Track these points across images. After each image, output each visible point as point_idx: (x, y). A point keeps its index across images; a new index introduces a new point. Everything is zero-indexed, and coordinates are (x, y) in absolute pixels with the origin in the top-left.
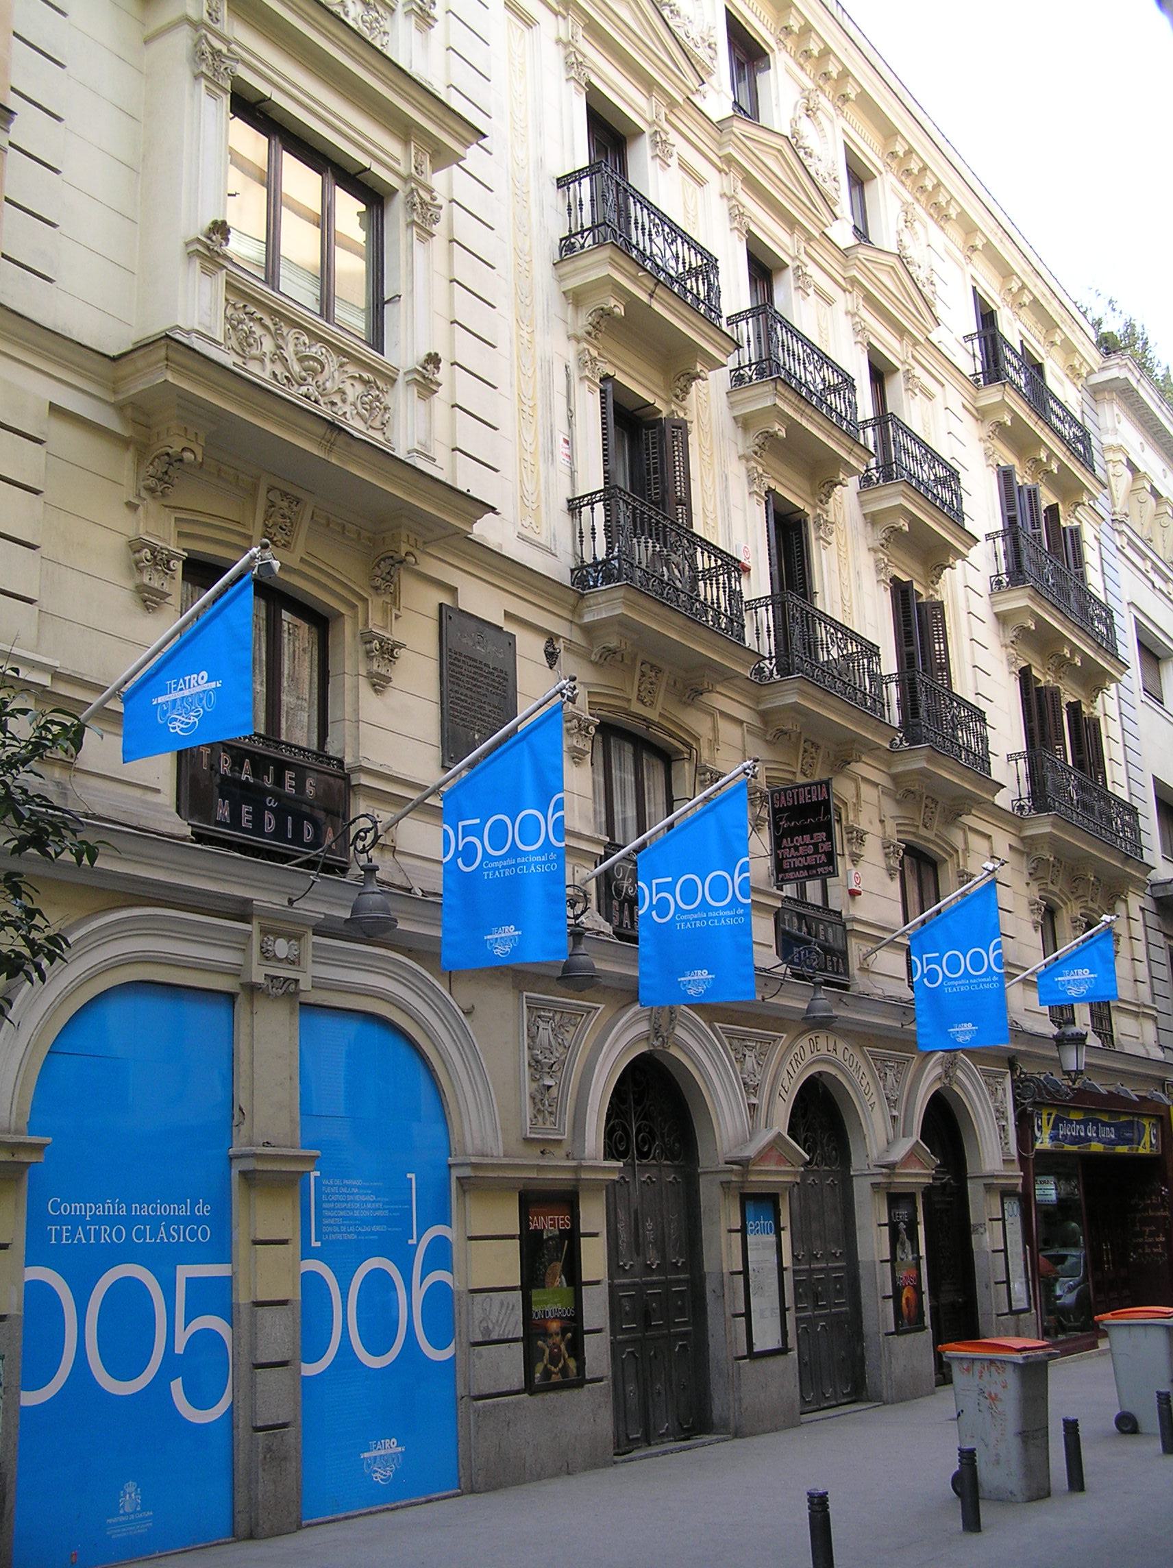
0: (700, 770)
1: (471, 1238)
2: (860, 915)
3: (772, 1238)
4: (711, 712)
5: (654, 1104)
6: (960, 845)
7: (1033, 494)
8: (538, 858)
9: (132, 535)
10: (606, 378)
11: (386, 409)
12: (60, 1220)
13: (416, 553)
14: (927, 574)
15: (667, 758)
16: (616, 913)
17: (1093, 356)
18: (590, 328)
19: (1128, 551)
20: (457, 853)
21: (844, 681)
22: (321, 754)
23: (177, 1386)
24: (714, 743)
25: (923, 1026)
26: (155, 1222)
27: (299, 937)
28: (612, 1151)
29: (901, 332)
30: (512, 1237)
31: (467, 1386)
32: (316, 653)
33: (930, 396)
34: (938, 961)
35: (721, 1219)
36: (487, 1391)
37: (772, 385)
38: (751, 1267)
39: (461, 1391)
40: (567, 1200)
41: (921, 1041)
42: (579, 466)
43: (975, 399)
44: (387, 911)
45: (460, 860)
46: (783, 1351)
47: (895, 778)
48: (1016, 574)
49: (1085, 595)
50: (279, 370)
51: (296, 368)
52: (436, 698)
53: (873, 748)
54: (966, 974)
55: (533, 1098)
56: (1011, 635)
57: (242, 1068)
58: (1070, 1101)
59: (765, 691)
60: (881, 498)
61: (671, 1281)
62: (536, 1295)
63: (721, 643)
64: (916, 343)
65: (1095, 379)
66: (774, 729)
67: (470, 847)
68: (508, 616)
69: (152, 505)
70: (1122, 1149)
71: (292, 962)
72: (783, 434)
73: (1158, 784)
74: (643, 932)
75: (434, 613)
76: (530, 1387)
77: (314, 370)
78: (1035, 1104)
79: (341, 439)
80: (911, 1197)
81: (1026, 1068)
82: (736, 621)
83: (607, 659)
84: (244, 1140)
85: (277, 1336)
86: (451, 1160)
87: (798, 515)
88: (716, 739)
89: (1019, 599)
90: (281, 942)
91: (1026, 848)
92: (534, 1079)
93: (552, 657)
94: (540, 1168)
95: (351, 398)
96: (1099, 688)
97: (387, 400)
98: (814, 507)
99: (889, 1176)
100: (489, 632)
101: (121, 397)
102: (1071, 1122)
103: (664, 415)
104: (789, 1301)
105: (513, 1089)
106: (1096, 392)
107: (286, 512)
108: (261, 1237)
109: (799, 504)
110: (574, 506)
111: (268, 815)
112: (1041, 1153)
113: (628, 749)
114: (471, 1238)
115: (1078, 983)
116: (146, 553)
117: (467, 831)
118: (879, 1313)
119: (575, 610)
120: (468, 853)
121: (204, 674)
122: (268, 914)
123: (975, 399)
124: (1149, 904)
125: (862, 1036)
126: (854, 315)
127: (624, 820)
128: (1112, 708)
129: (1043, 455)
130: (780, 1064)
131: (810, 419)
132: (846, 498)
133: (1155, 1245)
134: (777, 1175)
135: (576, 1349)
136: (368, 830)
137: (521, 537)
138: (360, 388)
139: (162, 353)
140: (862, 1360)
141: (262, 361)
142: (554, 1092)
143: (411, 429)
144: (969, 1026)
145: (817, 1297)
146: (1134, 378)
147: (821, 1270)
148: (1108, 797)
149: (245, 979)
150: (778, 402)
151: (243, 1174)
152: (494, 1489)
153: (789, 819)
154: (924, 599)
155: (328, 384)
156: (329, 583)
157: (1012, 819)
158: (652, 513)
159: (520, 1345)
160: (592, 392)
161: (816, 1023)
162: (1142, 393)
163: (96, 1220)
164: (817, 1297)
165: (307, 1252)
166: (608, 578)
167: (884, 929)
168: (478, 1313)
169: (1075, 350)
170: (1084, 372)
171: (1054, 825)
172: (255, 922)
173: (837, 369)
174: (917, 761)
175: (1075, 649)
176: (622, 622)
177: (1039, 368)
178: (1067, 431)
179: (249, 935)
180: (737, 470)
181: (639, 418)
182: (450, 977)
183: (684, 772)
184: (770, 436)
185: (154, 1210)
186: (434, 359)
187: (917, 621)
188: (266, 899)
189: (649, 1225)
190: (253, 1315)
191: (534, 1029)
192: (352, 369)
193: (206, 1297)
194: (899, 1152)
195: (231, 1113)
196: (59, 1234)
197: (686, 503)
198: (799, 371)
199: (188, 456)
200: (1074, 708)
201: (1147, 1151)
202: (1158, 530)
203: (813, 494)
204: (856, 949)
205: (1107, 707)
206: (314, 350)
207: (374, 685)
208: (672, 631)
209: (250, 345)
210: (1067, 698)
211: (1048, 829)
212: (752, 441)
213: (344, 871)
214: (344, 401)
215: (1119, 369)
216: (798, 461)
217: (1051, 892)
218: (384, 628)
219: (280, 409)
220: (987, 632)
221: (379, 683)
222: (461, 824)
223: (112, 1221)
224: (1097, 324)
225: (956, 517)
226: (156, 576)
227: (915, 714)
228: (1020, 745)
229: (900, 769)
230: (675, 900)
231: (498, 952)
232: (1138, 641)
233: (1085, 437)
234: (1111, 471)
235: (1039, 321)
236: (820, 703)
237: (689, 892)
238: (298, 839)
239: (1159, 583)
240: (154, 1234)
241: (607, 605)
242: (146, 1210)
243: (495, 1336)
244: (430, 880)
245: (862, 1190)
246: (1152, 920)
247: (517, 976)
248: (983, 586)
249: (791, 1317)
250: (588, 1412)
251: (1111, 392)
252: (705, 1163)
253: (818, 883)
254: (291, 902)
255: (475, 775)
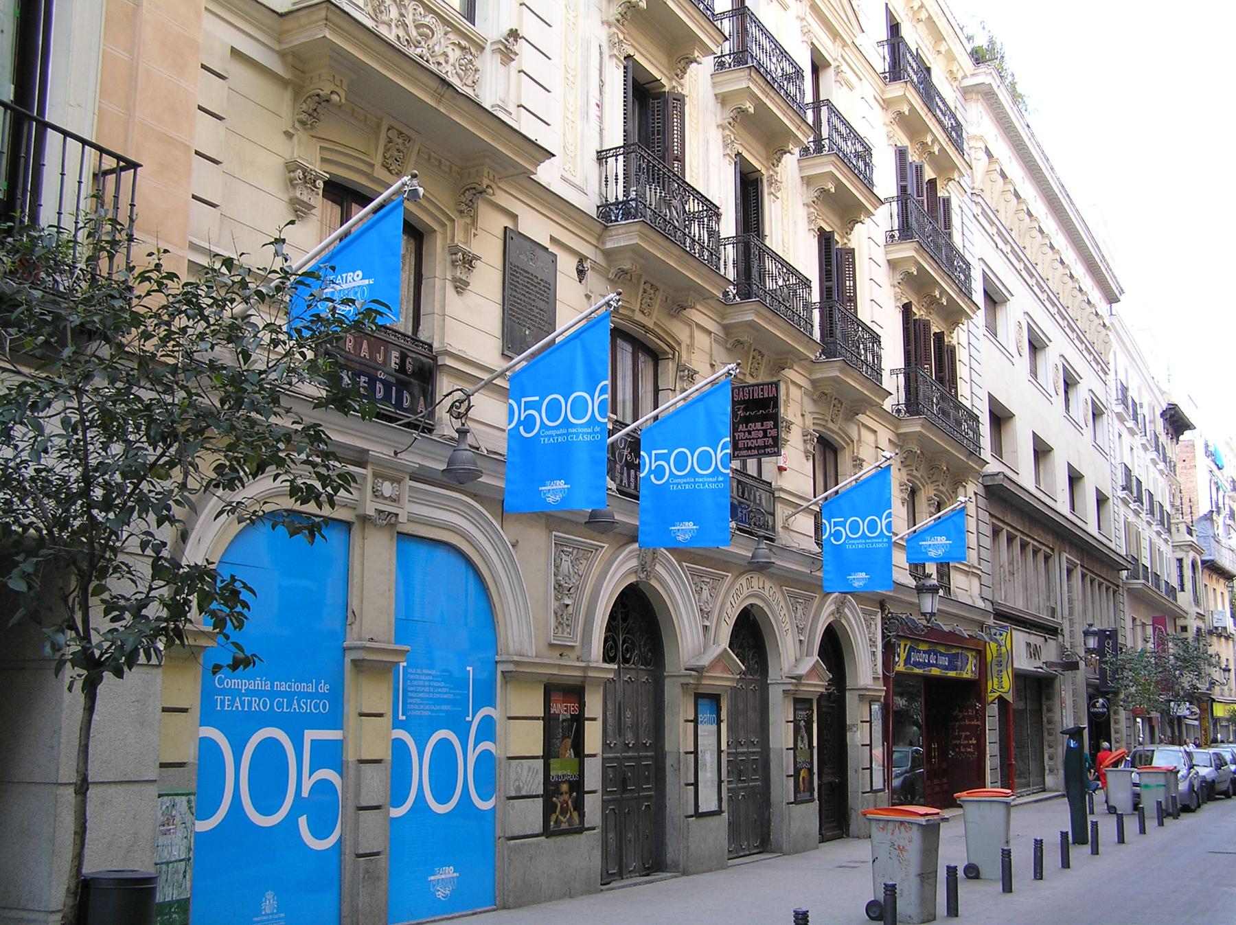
0: (680, 368)
1: (510, 718)
2: (786, 486)
3: (715, 727)
4: (689, 323)
5: (638, 622)
6: (855, 438)
7: (919, 170)
8: (586, 430)
9: (288, 158)
10: (628, 57)
11: (477, 70)
12: (223, 692)
13: (494, 186)
14: (843, 227)
15: (656, 357)
16: (618, 475)
17: (967, 63)
18: (619, 17)
19: (981, 218)
20: (519, 423)
21: (783, 305)
22: (415, 340)
23: (303, 821)
24: (691, 347)
25: (827, 574)
26: (290, 695)
27: (399, 481)
28: (608, 658)
29: (835, 35)
30: (538, 718)
31: (503, 830)
32: (413, 259)
33: (851, 88)
34: (843, 524)
35: (679, 709)
36: (516, 834)
37: (747, 71)
38: (698, 748)
39: (499, 833)
40: (576, 692)
41: (825, 584)
42: (606, 126)
43: (883, 92)
44: (475, 464)
45: (521, 428)
46: (718, 812)
47: (814, 382)
48: (906, 231)
49: (951, 247)
50: (401, 33)
51: (414, 33)
52: (499, 300)
53: (802, 358)
54: (864, 536)
55: (556, 613)
56: (899, 277)
57: (355, 581)
58: (925, 636)
59: (729, 310)
60: (815, 166)
61: (641, 757)
62: (554, 763)
63: (705, 270)
64: (845, 45)
65: (966, 83)
66: (735, 341)
67: (530, 418)
68: (552, 239)
69: (301, 135)
70: (952, 674)
71: (394, 500)
72: (752, 110)
73: (992, 399)
74: (643, 491)
75: (501, 235)
76: (547, 832)
77: (427, 36)
78: (898, 636)
79: (450, 92)
80: (810, 701)
81: (893, 609)
82: (715, 254)
83: (620, 278)
84: (355, 636)
85: (375, 785)
86: (498, 658)
87: (754, 176)
88: (692, 345)
89: (907, 251)
90: (387, 484)
91: (900, 442)
92: (557, 599)
93: (581, 273)
94: (560, 666)
95: (451, 60)
96: (956, 324)
97: (477, 63)
98: (768, 169)
99: (796, 685)
100: (538, 251)
101: (284, 47)
102: (919, 651)
103: (667, 89)
104: (724, 776)
105: (545, 605)
106: (966, 92)
107: (401, 147)
108: (366, 711)
109: (658, 76)
110: (602, 157)
111: (379, 385)
112: (898, 673)
113: (629, 348)
114: (510, 718)
115: (936, 547)
116: (299, 173)
117: (528, 406)
118: (783, 787)
119: (600, 238)
120: (529, 423)
121: (360, 272)
122: (379, 462)
123: (883, 92)
124: (981, 490)
125: (785, 580)
126: (803, 19)
127: (624, 402)
128: (964, 341)
129: (929, 140)
130: (725, 596)
131: (772, 100)
132: (790, 164)
133: (969, 746)
134: (721, 681)
135: (579, 806)
136: (462, 402)
137: (563, 178)
138: (458, 52)
139: (323, 14)
140: (769, 821)
141: (390, 26)
142: (570, 608)
143: (493, 87)
144: (863, 575)
145: (740, 773)
146: (994, 82)
147: (743, 753)
148: (959, 406)
149: (360, 512)
150: (751, 85)
151: (355, 662)
152: (520, 906)
153: (745, 410)
154: (839, 246)
155: (436, 48)
156: (431, 209)
157: (892, 419)
158: (656, 163)
159: (541, 800)
160: (618, 67)
161: (757, 567)
162: (1000, 96)
163: (250, 692)
164: (740, 773)
165: (397, 724)
166: (627, 215)
167: (801, 498)
168: (513, 776)
169: (954, 59)
170: (959, 76)
171: (923, 426)
172: (369, 468)
173: (792, 63)
174: (832, 370)
175: (943, 292)
176: (635, 250)
177: (928, 70)
178: (947, 122)
179: (365, 477)
180: (716, 136)
181: (647, 90)
182: (503, 516)
183: (668, 370)
184: (742, 111)
185: (290, 687)
186: (514, 34)
187: (835, 260)
188: (379, 450)
189: (628, 714)
190: (358, 771)
191: (558, 561)
192: (454, 37)
193: (327, 754)
194: (803, 669)
195: (347, 614)
196: (223, 702)
197: (681, 159)
198: (764, 59)
199: (335, 97)
200: (939, 337)
201: (968, 676)
202: (1003, 204)
203: (768, 159)
204: (781, 511)
205: (959, 337)
206: (428, 19)
207: (456, 288)
208: (669, 258)
209: (381, 12)
210: (935, 329)
211: (918, 429)
212: (728, 114)
213: (430, 431)
214: (447, 62)
215: (985, 76)
216: (759, 129)
217: (915, 477)
218: (466, 243)
219: (406, 65)
220: (882, 274)
221: (461, 286)
222: (524, 400)
223: (259, 694)
224: (969, 39)
225: (868, 185)
226: (305, 192)
227: (832, 334)
228: (901, 364)
229: (818, 376)
230: (669, 467)
231: (550, 500)
232: (985, 291)
233: (958, 127)
234: (973, 156)
235: (930, 34)
236: (770, 322)
237: (681, 462)
238: (399, 405)
239: (1001, 244)
240: (289, 705)
241: (625, 236)
242: (284, 687)
243: (524, 793)
244: (500, 444)
245: (775, 695)
246: (982, 502)
247: (551, 520)
248: (881, 239)
249: (724, 787)
250: (585, 851)
251: (978, 92)
252: (669, 668)
253: (755, 460)
254: (396, 453)
255: (533, 365)
